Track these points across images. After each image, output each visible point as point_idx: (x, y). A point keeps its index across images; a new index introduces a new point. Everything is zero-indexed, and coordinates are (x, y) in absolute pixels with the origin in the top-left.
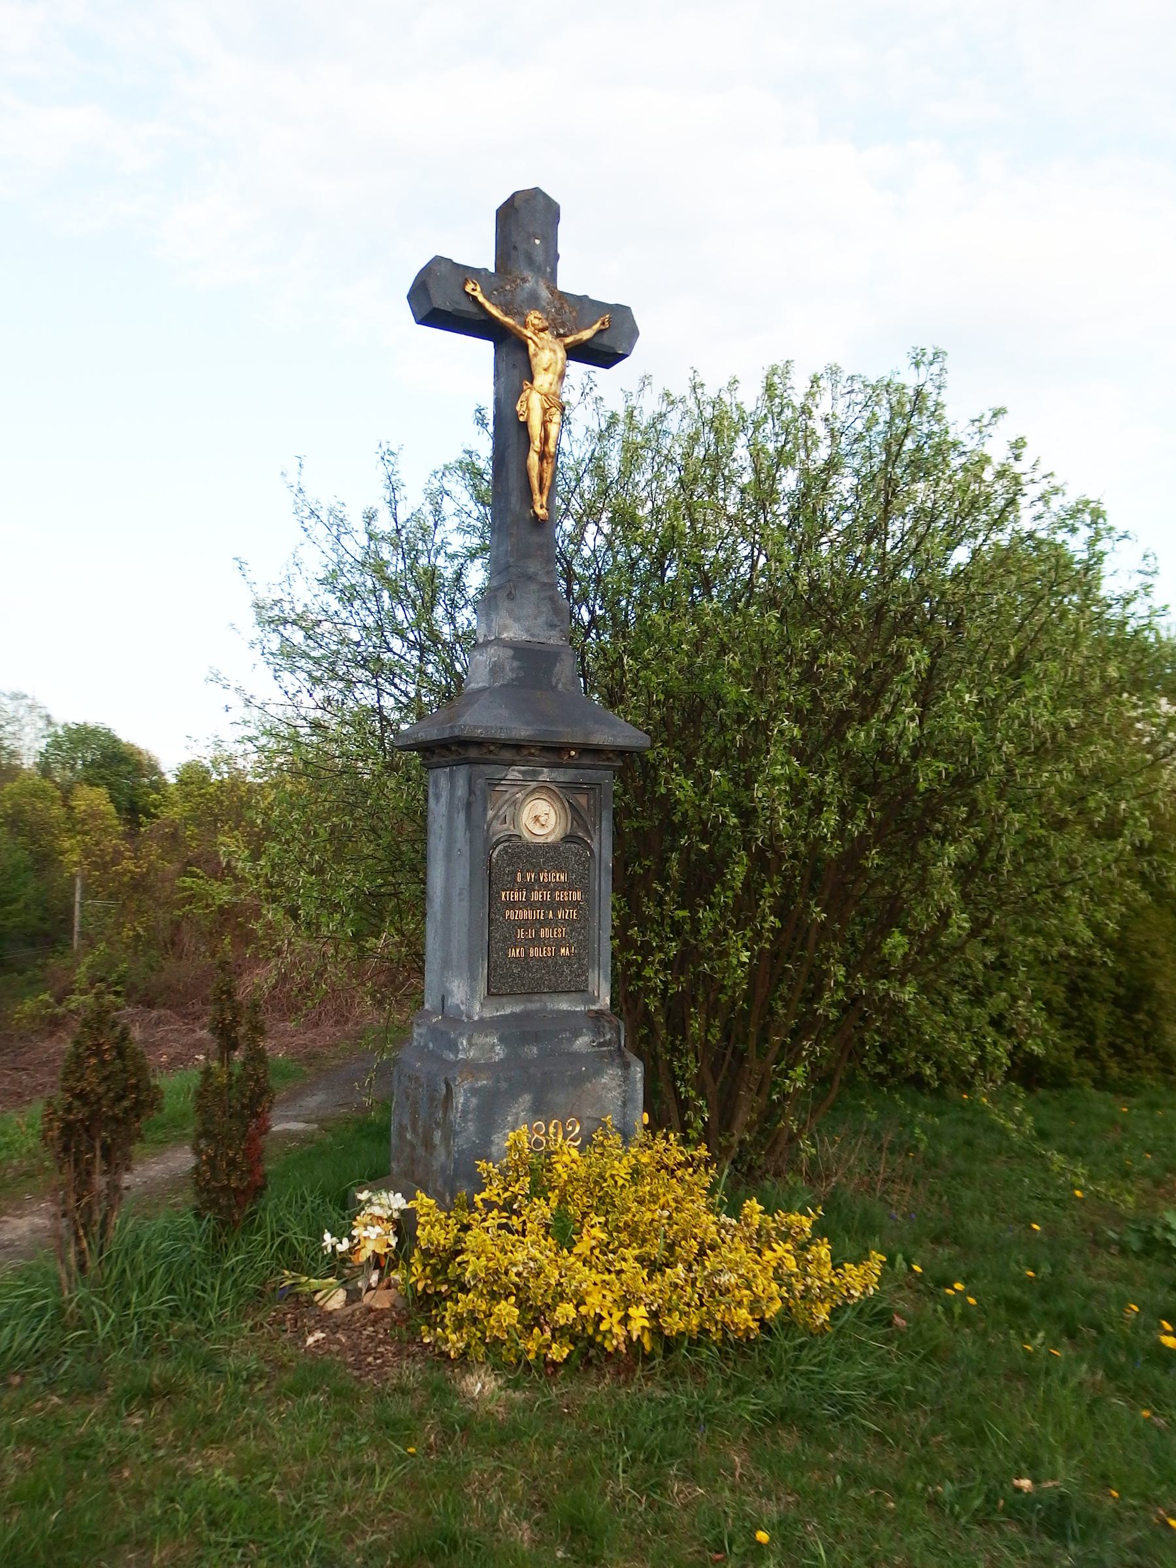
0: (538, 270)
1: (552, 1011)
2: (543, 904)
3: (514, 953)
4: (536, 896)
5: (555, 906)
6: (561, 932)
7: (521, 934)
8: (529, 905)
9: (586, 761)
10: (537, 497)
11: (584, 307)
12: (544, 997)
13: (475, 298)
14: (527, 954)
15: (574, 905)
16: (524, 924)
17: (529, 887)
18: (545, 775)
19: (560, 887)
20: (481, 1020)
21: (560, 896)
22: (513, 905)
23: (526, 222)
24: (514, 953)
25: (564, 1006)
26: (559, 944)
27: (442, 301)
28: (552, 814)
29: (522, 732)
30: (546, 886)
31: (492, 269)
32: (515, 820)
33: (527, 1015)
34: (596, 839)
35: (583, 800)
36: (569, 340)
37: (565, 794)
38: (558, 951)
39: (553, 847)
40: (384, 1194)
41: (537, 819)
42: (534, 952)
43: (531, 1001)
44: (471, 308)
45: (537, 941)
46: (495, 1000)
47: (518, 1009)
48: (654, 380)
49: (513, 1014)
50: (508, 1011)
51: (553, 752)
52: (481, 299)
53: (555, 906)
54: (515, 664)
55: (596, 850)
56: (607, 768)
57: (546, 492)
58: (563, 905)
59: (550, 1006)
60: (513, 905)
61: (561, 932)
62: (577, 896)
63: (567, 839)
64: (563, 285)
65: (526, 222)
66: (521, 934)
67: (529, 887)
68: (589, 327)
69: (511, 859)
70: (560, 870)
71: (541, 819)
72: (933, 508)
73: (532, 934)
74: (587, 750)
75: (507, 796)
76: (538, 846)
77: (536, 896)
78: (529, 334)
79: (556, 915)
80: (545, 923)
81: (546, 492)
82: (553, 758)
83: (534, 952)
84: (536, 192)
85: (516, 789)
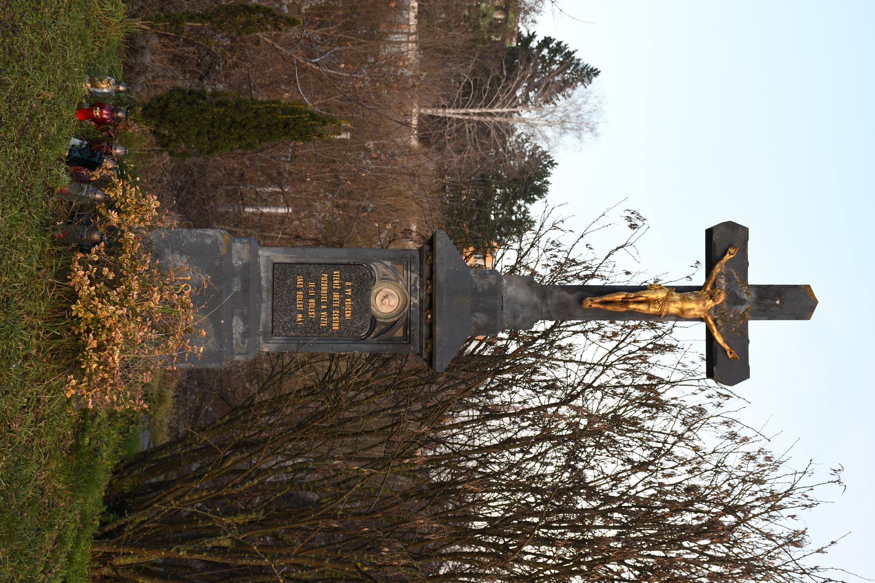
1: (260, 307)
2: (331, 301)
3: (300, 280)
4: (336, 296)
6: (312, 314)
7: (312, 285)
8: (331, 291)
9: (425, 329)
10: (598, 300)
11: (741, 342)
12: (270, 303)
13: (725, 254)
14: (299, 289)
15: (330, 325)
16: (318, 288)
17: (342, 291)
19: (342, 315)
20: (258, 256)
21: (336, 313)
22: (330, 280)
23: (792, 302)
24: (300, 280)
26: (305, 312)
27: (725, 244)
28: (391, 310)
30: (342, 303)
32: (385, 279)
33: (260, 288)
35: (399, 333)
37: (404, 319)
38: (300, 312)
39: (368, 309)
40: (177, 256)
41: (386, 297)
46: (271, 267)
47: (263, 282)
48: (536, 25)
49: (260, 278)
50: (263, 275)
51: (429, 304)
54: (487, 287)
55: (366, 341)
56: (421, 348)
58: (330, 315)
59: (264, 305)
60: (330, 280)
61: (312, 314)
62: (336, 327)
63: (374, 319)
65: (792, 302)
66: (312, 285)
67: (342, 291)
68: (725, 342)
70: (353, 314)
71: (387, 302)
73: (312, 293)
74: (431, 325)
75: (401, 276)
76: (369, 298)
77: (336, 296)
79: (324, 310)
80: (318, 303)
82: (425, 305)
85: (405, 283)
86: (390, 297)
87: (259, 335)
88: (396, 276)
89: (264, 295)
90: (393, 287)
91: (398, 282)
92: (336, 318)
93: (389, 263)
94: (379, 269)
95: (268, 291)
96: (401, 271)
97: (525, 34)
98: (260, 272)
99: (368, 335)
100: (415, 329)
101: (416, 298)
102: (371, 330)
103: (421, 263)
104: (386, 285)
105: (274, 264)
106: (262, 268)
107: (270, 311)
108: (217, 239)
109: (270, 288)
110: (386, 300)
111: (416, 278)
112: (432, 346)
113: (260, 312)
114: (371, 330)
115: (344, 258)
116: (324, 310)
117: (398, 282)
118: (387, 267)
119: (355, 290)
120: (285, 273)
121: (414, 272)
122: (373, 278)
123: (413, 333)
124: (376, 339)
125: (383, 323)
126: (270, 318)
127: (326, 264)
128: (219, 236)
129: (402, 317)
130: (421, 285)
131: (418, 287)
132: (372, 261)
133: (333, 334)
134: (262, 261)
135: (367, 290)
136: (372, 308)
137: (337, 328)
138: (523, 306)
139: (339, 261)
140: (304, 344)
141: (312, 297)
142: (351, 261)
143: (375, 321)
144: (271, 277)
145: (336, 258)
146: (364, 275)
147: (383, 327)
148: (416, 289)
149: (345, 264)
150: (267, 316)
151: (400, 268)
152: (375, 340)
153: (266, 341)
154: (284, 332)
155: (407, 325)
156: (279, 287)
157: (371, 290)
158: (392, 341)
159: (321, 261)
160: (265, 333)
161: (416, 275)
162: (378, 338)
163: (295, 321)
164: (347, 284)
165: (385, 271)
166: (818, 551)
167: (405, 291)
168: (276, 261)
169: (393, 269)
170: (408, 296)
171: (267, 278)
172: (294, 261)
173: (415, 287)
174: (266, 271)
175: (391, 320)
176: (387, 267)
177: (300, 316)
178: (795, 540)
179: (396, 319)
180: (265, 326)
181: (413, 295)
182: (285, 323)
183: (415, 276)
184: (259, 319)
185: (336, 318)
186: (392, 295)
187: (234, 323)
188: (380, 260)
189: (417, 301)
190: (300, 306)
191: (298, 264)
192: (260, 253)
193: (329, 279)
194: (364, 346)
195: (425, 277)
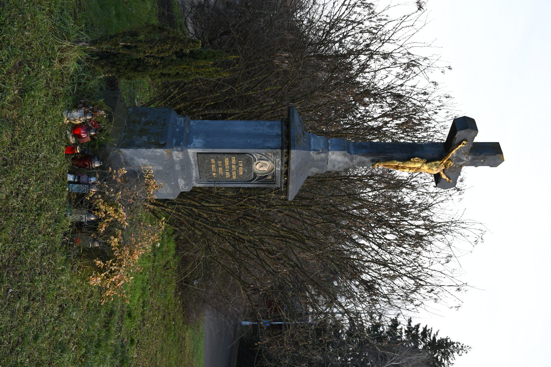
0: (471, 161)
5: (231, 171)
8: (230, 165)
15: (231, 176)
16: (223, 163)
23: (491, 153)
29: (293, 166)
30: (238, 169)
31: (477, 140)
33: (191, 164)
34: (256, 182)
35: (270, 177)
36: (442, 173)
38: (214, 172)
42: (213, 166)
43: (195, 165)
44: (457, 141)
45: (217, 167)
47: (192, 162)
49: (191, 161)
52: (460, 146)
53: (231, 171)
58: (231, 174)
60: (230, 160)
62: (234, 177)
63: (255, 175)
64: (465, 169)
65: (491, 153)
72: (375, 288)
77: (233, 166)
78: (444, 162)
80: (224, 168)
83: (213, 166)
84: (503, 160)
89: (194, 167)
92: (234, 173)
103: (282, 156)
108: (163, 153)
112: (289, 115)
128: (164, 152)
130: (282, 165)
138: (339, 162)
148: (279, 165)
178: (431, 243)
185: (234, 173)
187: (179, 181)
195: (284, 162)
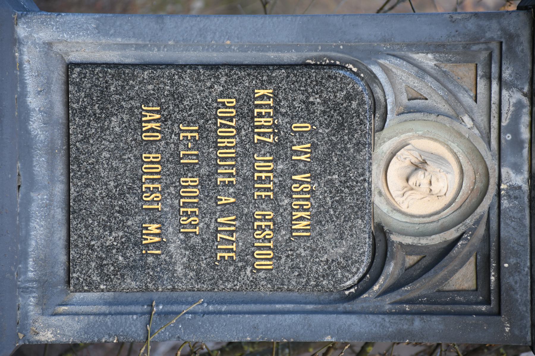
1: (27, 202)
3: (151, 119)
8: (247, 150)
12: (59, 189)
15: (246, 256)
16: (208, 137)
17: (281, 149)
18: (517, 179)
19: (282, 223)
22: (246, 114)
24: (151, 119)
25: (493, 278)
30: (284, 188)
35: (464, 278)
39: (363, 205)
41: (419, 166)
45: (175, 168)
46: (58, 75)
47: (36, 126)
50: (34, 102)
55: (357, 305)
57: (175, 308)
58: (247, 223)
59: (39, 198)
60: (246, 114)
62: (264, 261)
66: (189, 132)
67: (281, 149)
69: (336, 107)
70: (317, 220)
75: (468, 100)
77: (263, 164)
79: (226, 210)
80: (209, 187)
81: (175, 308)
85: (482, 119)
86: (432, 167)
87: (26, 290)
88: (453, 98)
89: (40, 165)
90: (443, 135)
91: (457, 117)
92: (264, 233)
93: (427, 60)
94: (396, 79)
95: (51, 152)
96: (468, 82)
97: (219, 352)
98: (24, 95)
99: (364, 285)
100: (516, 268)
101: (517, 169)
102: (375, 270)
104: (420, 127)
105: (70, 67)
106: (31, 83)
107: (59, 214)
109: (59, 142)
110: (420, 177)
111: (519, 105)
113: (28, 219)
114: (375, 270)
115: (287, 47)
116: (226, 210)
117: (457, 117)
118: (422, 71)
119: (322, 148)
120: (104, 93)
121: (510, 86)
122: (379, 110)
123: (508, 280)
124: (388, 299)
125: (410, 249)
126: (60, 234)
127: (231, 66)
129: (472, 230)
131: (525, 134)
132: (374, 54)
133: (255, 282)
134: (29, 58)
135: (359, 146)
136: (376, 199)
137: (268, 265)
139: (272, 56)
140: (167, 314)
141: (190, 169)
142: (308, 55)
143: (387, 241)
144: (59, 109)
145: (263, 48)
146: (349, 98)
147: (411, 260)
148: (517, 143)
149: (290, 66)
150: (51, 233)
151: (465, 72)
152: (387, 303)
153: (47, 308)
154: (106, 278)
155: (490, 254)
156: (86, 139)
157: (371, 146)
158: (442, 303)
159: (216, 57)
160: (44, 285)
161: (517, 96)
162: (395, 296)
163: (138, 244)
164: (297, 126)
165: (415, 83)
166: (431, 182)
167: (482, 147)
168: (75, 57)
169: (442, 78)
170: (492, 164)
171: (48, 112)
172: (130, 57)
173: (516, 133)
174: (45, 90)
175: (437, 240)
176: (422, 71)
177: (153, 228)
179: (451, 235)
180: (44, 262)
181: (509, 158)
182: (108, 249)
183: (513, 98)
184: (25, 240)
185: (264, 233)
186: (440, 159)
188: (401, 49)
189: (520, 180)
190: (153, 199)
191: (144, 66)
192: (21, 31)
193: (240, 115)
194: (353, 319)
